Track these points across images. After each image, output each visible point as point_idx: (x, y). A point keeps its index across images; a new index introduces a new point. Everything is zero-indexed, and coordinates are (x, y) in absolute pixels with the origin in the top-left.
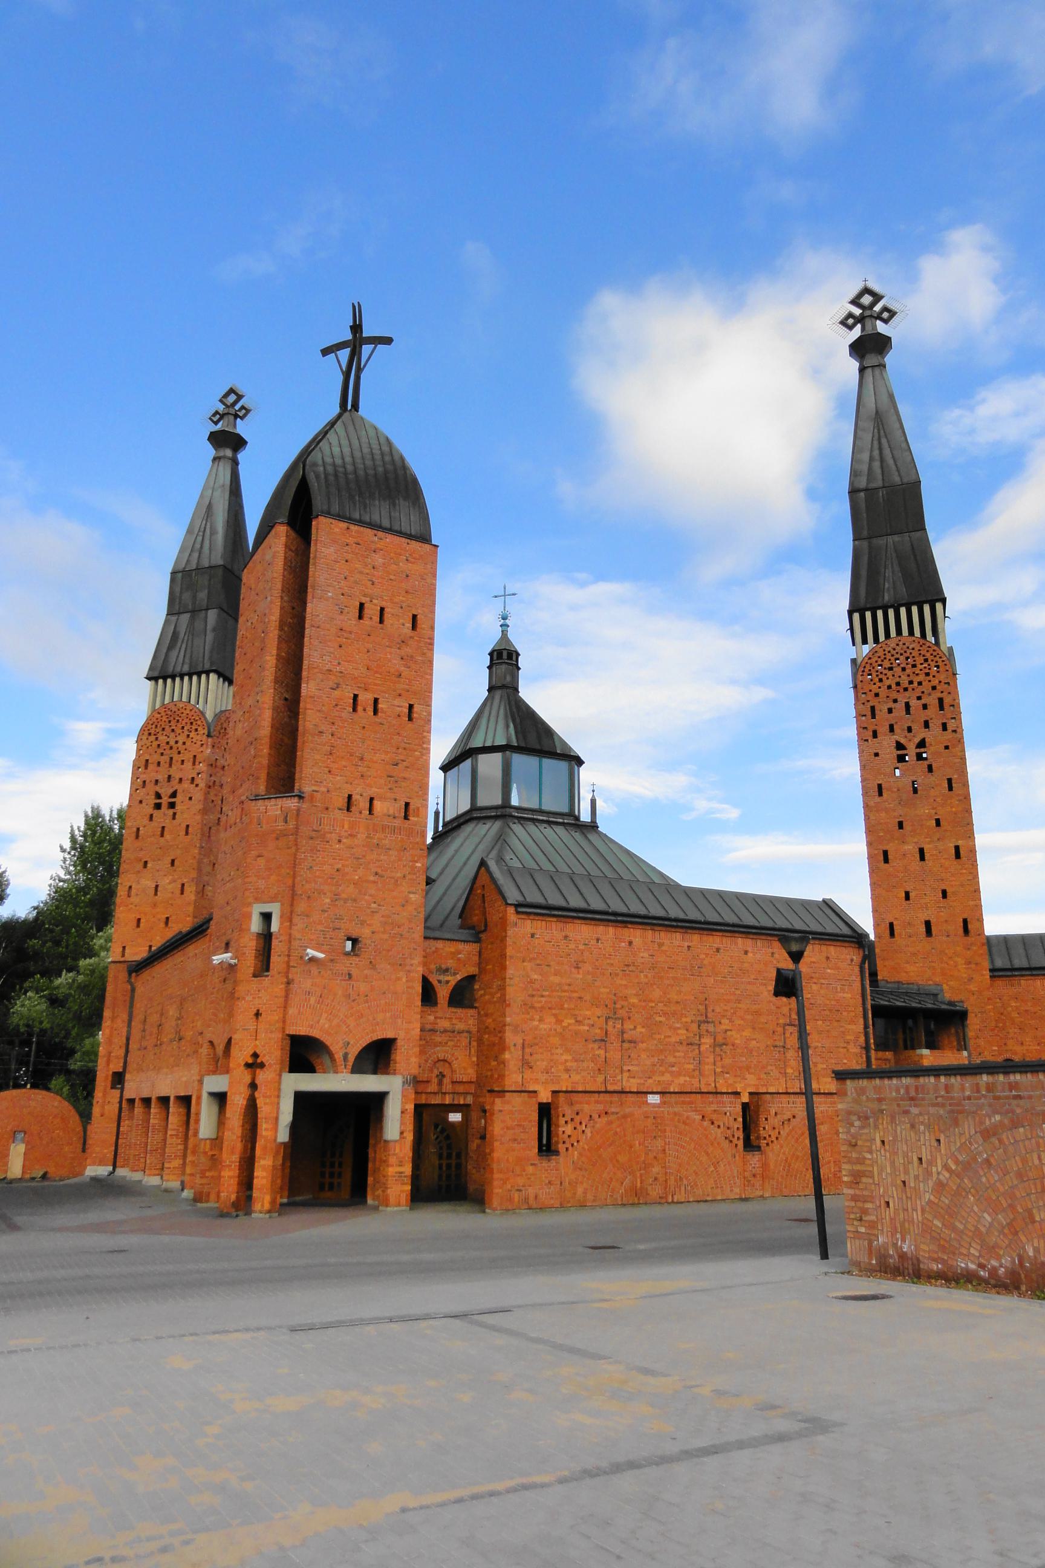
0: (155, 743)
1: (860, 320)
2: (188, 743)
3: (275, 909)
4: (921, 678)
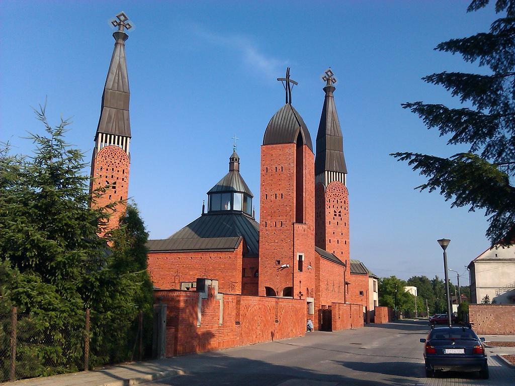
0: (105, 161)
4: (341, 194)
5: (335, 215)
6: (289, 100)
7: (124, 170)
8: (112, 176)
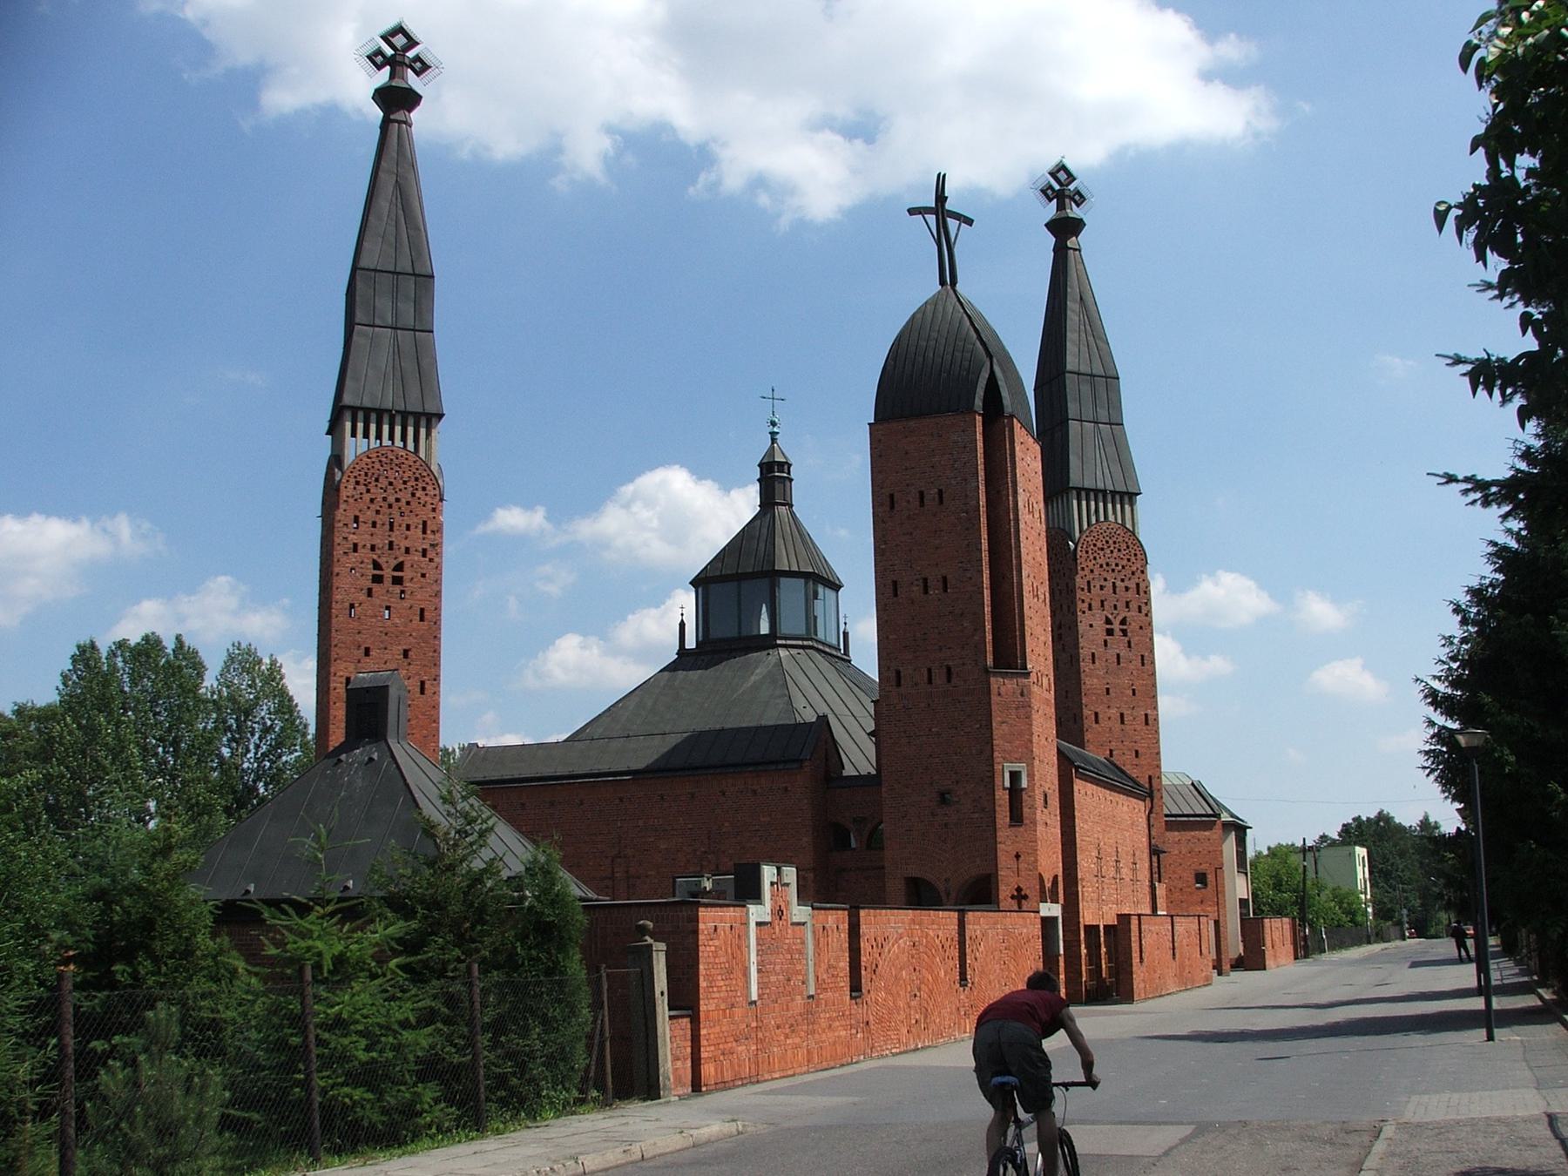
0: (367, 497)
1: (389, 61)
2: (414, 504)
3: (1021, 767)
5: (1110, 632)
6: (948, 275)
7: (425, 523)
8: (391, 543)
